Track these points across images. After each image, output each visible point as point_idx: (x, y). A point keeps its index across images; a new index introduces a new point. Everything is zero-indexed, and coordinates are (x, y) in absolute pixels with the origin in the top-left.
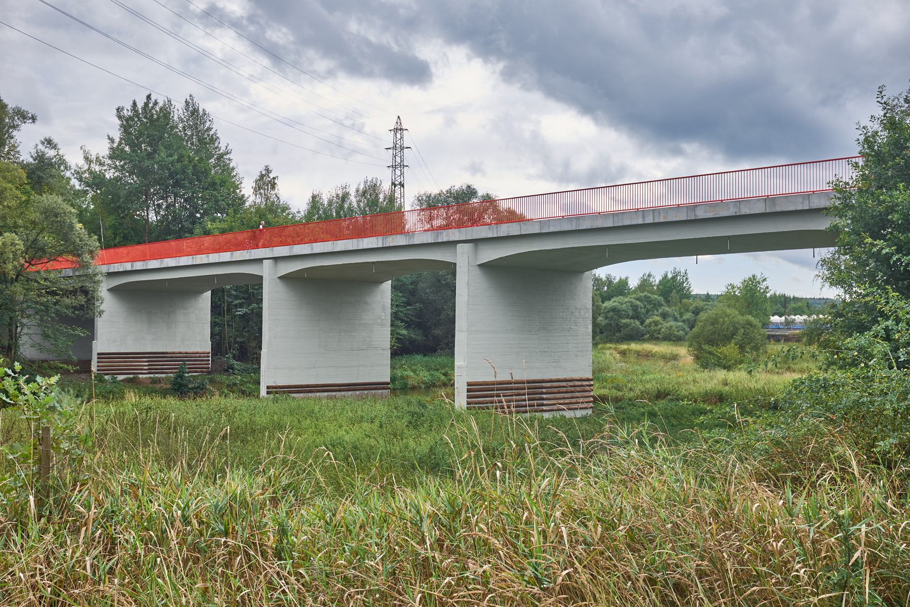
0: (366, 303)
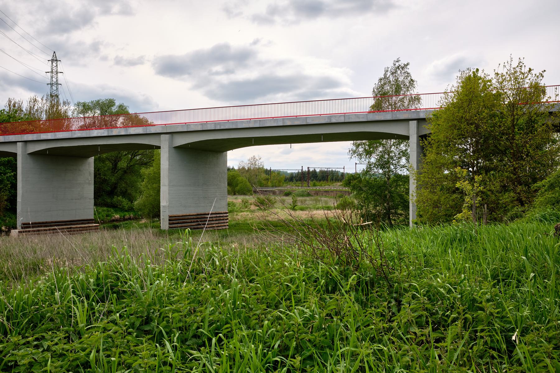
0: (80, 170)
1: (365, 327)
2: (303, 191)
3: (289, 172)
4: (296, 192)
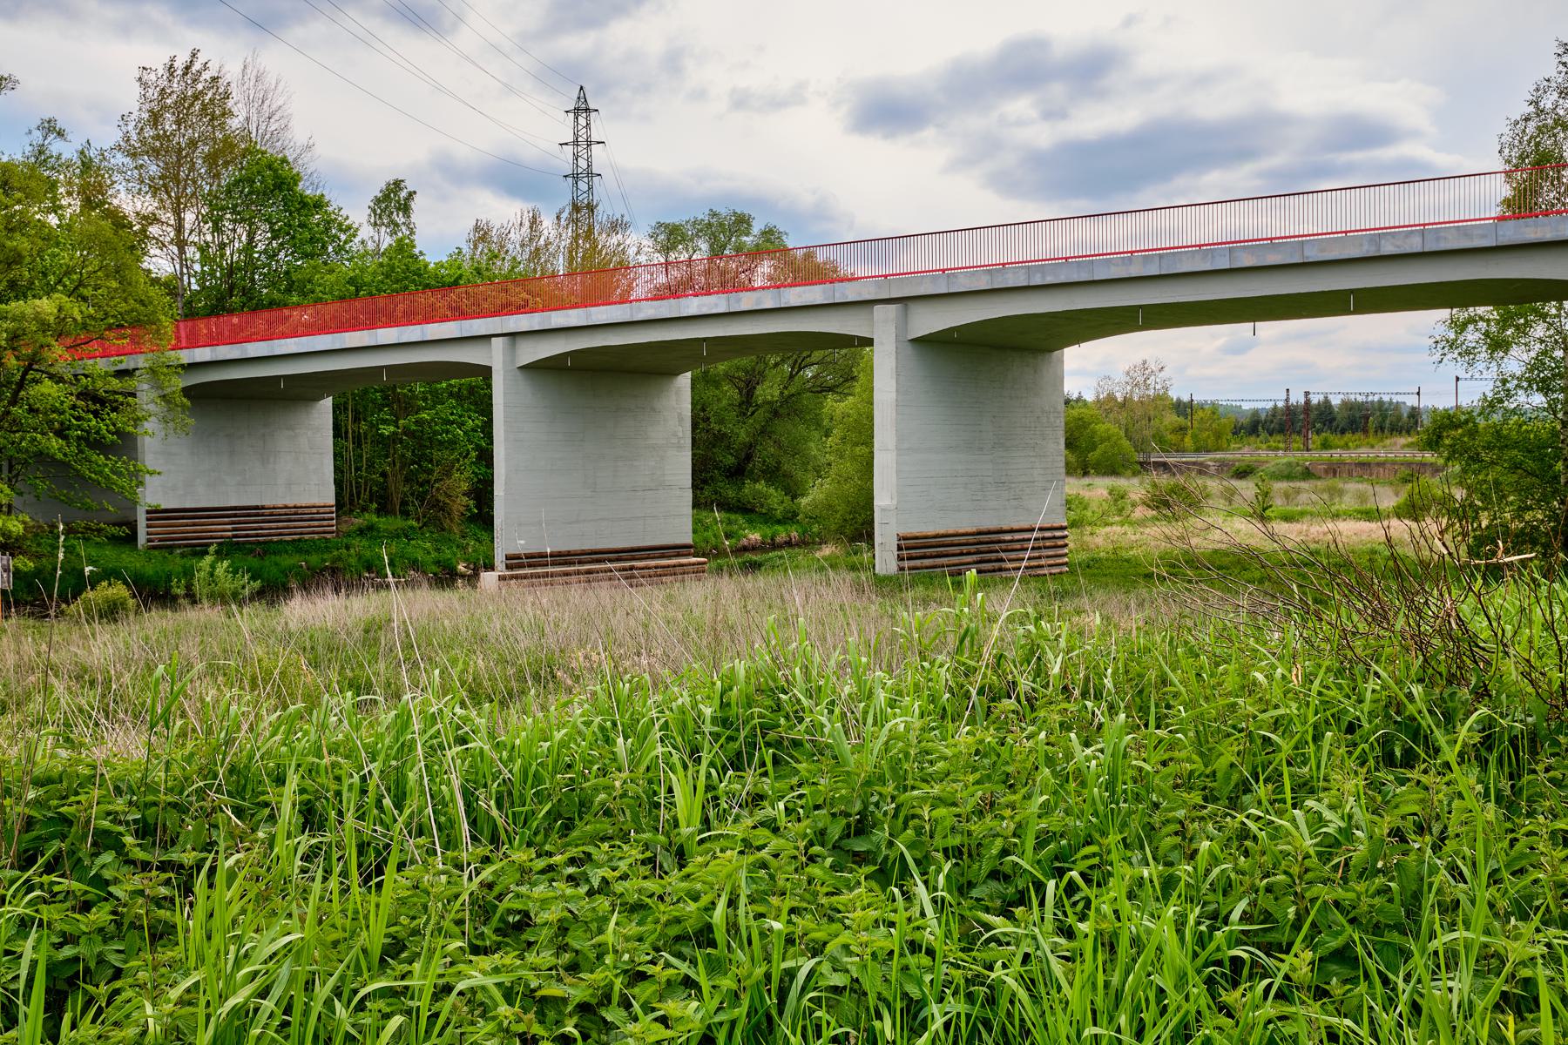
0: (653, 410)
1: (1513, 874)
2: (1289, 464)
3: (1246, 406)
4: (1270, 467)
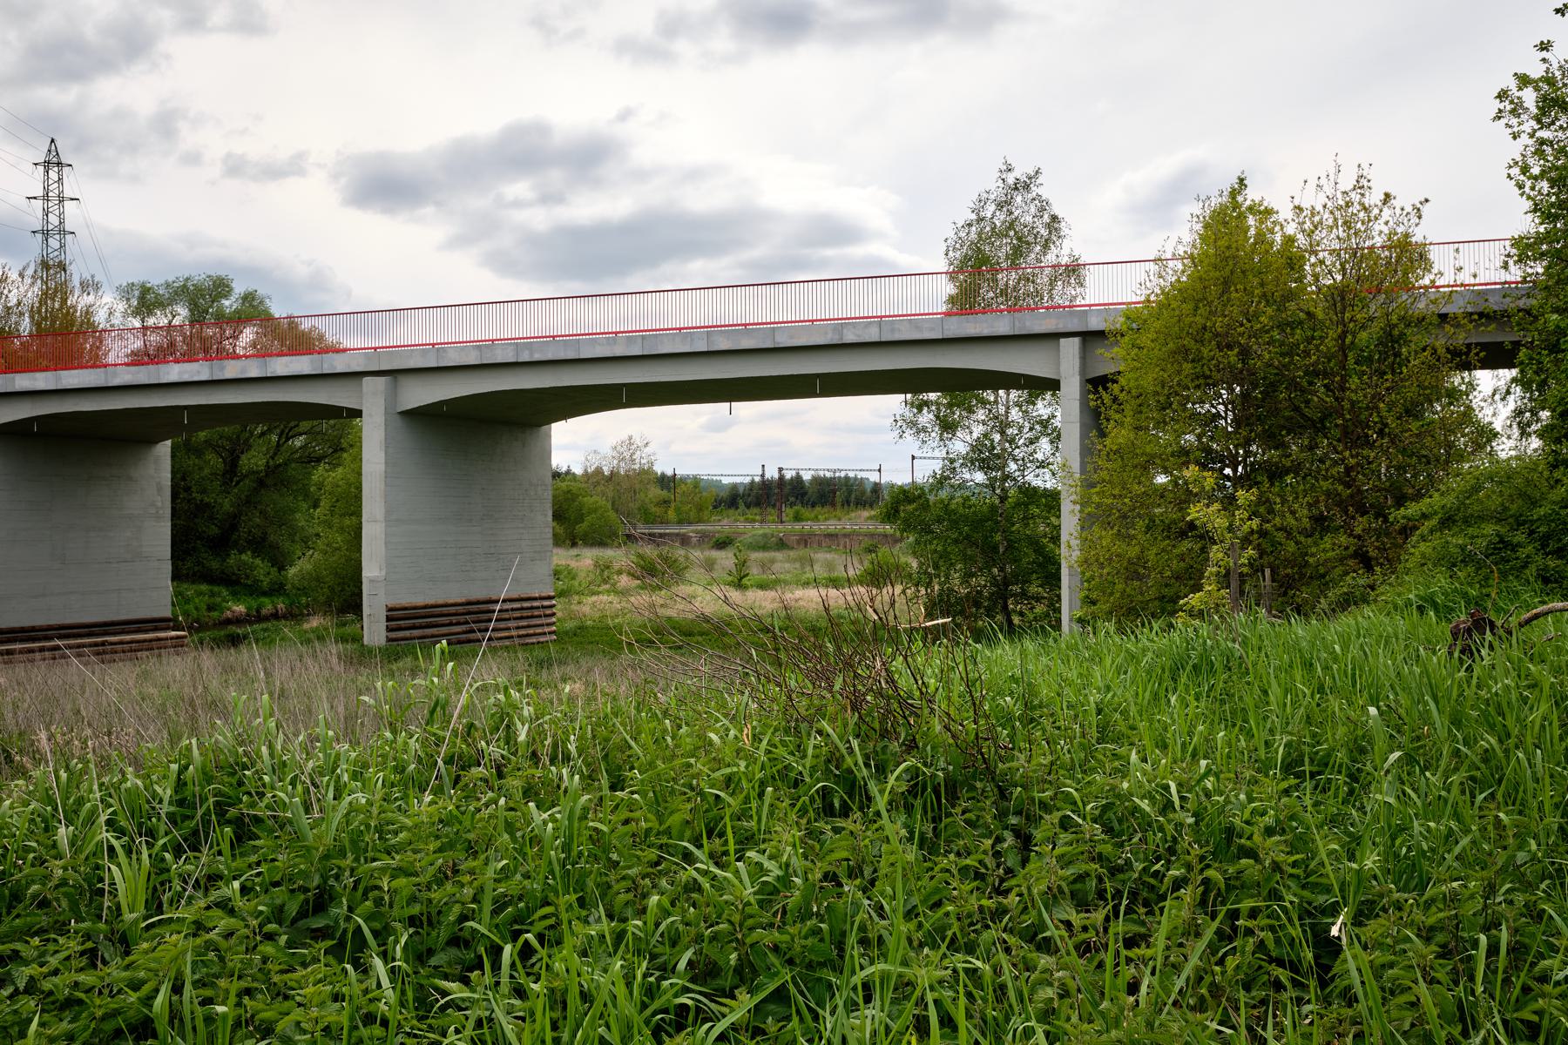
2: (765, 535)
3: (726, 481)
4: (748, 538)
